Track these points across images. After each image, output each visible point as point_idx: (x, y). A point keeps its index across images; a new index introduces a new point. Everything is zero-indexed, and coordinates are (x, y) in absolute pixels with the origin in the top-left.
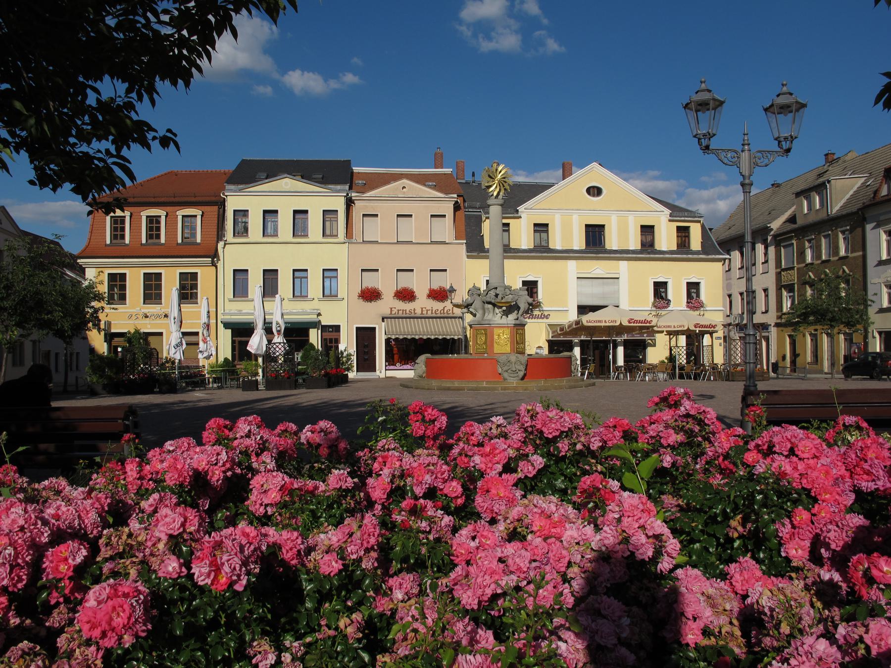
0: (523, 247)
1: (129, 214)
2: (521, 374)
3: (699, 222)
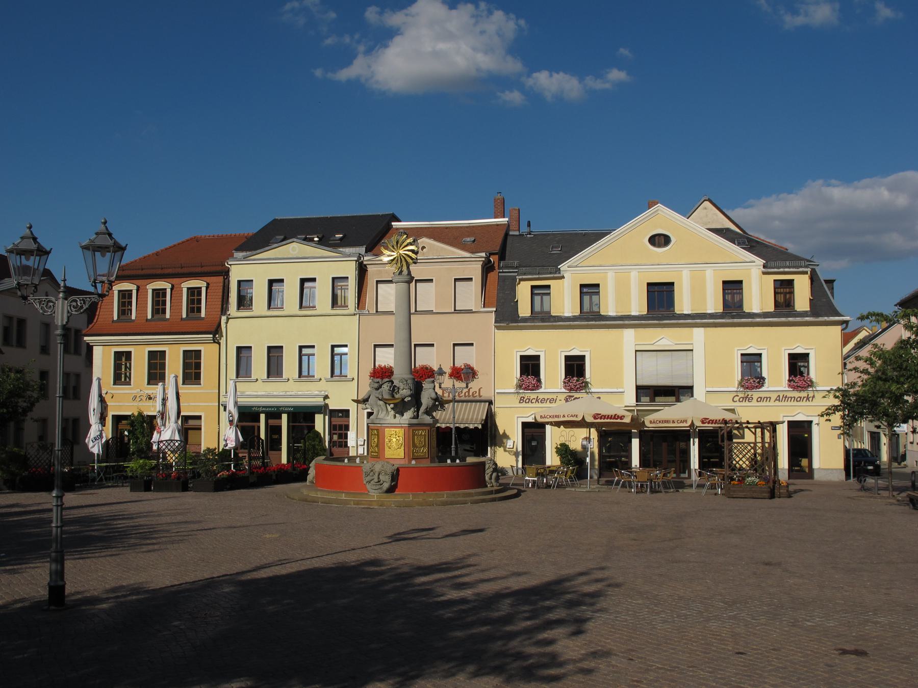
0: (567, 315)
1: (205, 284)
2: (386, 486)
3: (806, 273)
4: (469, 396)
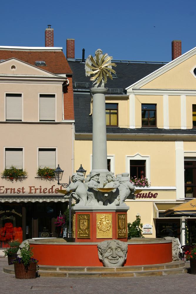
2: (121, 260)
4: (52, 192)
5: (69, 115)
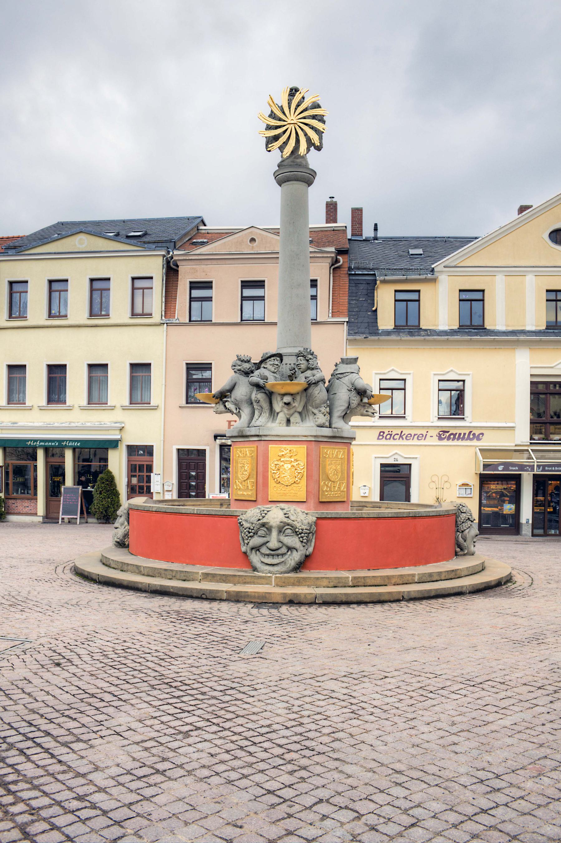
5: (341, 311)
